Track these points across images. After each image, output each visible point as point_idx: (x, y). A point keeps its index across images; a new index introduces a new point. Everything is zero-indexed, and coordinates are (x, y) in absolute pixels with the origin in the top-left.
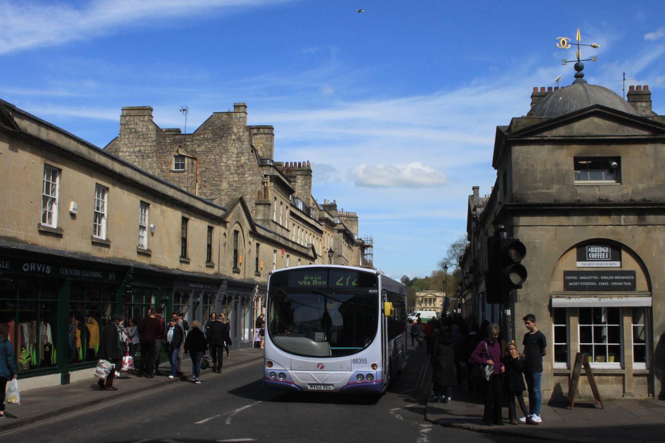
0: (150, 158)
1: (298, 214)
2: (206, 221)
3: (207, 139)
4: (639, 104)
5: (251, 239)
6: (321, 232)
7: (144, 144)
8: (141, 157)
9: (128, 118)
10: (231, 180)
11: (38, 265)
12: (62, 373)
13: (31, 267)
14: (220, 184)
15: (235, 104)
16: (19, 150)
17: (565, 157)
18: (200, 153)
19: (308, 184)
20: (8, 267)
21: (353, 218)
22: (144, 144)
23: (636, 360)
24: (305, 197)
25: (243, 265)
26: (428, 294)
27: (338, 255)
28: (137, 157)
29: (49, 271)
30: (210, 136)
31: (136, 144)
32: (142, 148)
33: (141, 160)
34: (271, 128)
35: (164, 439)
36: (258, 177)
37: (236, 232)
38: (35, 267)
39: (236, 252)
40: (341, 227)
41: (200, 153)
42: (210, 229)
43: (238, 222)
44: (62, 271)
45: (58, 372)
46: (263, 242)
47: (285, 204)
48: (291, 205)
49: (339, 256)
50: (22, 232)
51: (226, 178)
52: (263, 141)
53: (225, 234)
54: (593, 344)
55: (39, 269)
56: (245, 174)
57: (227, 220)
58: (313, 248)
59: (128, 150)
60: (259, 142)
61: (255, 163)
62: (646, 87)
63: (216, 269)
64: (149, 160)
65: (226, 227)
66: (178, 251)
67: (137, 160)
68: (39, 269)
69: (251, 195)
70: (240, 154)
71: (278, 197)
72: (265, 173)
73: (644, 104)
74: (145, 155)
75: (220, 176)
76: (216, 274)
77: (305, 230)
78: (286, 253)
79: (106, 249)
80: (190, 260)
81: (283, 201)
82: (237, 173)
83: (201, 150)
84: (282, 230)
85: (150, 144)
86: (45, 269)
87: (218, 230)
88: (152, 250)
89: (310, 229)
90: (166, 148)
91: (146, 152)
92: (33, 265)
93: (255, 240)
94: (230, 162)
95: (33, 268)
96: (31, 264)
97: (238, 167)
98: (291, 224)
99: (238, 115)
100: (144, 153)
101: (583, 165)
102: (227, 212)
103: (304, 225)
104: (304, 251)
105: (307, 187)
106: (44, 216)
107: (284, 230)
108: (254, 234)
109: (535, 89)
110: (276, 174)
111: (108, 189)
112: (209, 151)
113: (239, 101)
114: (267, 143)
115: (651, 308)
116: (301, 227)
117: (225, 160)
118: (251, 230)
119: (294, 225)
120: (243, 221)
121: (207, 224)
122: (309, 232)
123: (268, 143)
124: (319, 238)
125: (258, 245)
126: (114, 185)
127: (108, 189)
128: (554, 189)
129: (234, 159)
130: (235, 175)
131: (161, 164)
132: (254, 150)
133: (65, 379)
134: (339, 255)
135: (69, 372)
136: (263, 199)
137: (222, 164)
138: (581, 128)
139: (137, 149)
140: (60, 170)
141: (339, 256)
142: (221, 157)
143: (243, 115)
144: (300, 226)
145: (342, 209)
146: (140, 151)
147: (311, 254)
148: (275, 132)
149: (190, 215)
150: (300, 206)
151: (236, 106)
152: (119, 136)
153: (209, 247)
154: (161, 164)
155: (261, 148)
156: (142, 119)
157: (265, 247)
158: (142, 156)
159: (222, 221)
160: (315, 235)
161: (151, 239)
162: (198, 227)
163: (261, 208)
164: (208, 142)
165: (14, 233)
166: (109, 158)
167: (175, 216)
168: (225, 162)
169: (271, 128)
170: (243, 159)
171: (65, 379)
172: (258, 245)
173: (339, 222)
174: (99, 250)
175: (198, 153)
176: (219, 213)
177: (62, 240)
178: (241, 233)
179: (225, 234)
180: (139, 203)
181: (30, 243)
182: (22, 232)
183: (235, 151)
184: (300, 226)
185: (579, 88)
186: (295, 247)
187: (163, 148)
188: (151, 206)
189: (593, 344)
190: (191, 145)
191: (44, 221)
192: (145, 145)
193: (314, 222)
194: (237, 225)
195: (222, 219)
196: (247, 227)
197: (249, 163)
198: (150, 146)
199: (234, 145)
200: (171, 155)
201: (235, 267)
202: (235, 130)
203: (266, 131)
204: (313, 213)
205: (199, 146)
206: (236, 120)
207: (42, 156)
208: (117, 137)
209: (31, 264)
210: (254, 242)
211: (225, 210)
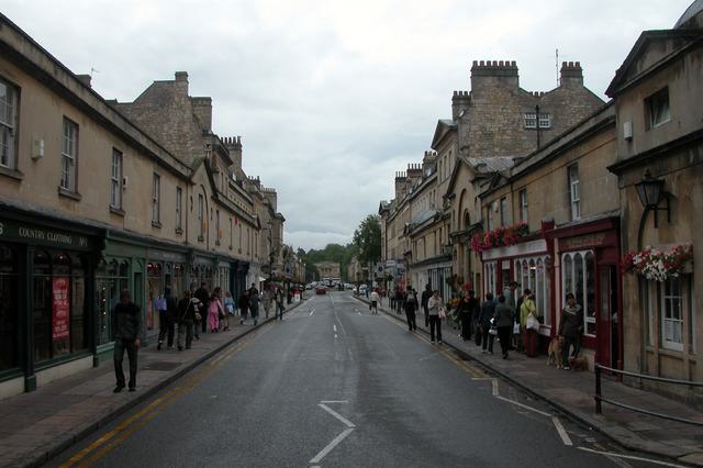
3: (149, 109)
4: (572, 79)
26: (326, 264)
34: (209, 100)
40: (266, 201)
45: (20, 376)
60: (200, 113)
73: (577, 80)
94: (171, 132)
97: (180, 137)
99: (180, 84)
109: (475, 62)
117: (166, 129)
125: (157, 225)
133: (30, 386)
142: (162, 128)
143: (185, 83)
148: (212, 104)
169: (209, 100)
170: (186, 128)
171: (30, 386)
174: (68, 206)
180: (111, 149)
196: (209, 193)
202: (176, 99)
203: (205, 103)
205: (140, 115)
210: (215, 208)
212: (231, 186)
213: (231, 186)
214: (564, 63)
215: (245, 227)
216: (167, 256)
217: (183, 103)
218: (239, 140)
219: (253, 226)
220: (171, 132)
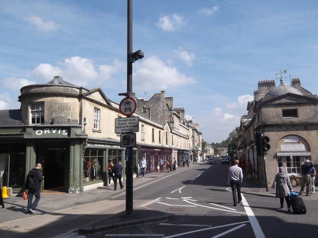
1: (182, 124)
17: (279, 110)
19: (183, 115)
21: (197, 125)
23: (288, 173)
35: (58, 209)
39: (167, 138)
54: (90, 156)
62: (298, 79)
70: (163, 106)
101: (286, 113)
106: (94, 126)
108: (171, 132)
109: (259, 81)
112: (153, 106)
115: (310, 156)
125: (143, 140)
128: (276, 120)
132: (167, 105)
138: (284, 101)
153: (160, 137)
157: (174, 136)
159: (163, 129)
162: (157, 131)
167: (151, 127)
185: (282, 87)
186: (183, 136)
189: (90, 156)
191: (94, 127)
201: (167, 143)
204: (186, 124)
210: (171, 134)
214: (293, 79)
215: (182, 139)
216: (114, 147)
219: (186, 138)
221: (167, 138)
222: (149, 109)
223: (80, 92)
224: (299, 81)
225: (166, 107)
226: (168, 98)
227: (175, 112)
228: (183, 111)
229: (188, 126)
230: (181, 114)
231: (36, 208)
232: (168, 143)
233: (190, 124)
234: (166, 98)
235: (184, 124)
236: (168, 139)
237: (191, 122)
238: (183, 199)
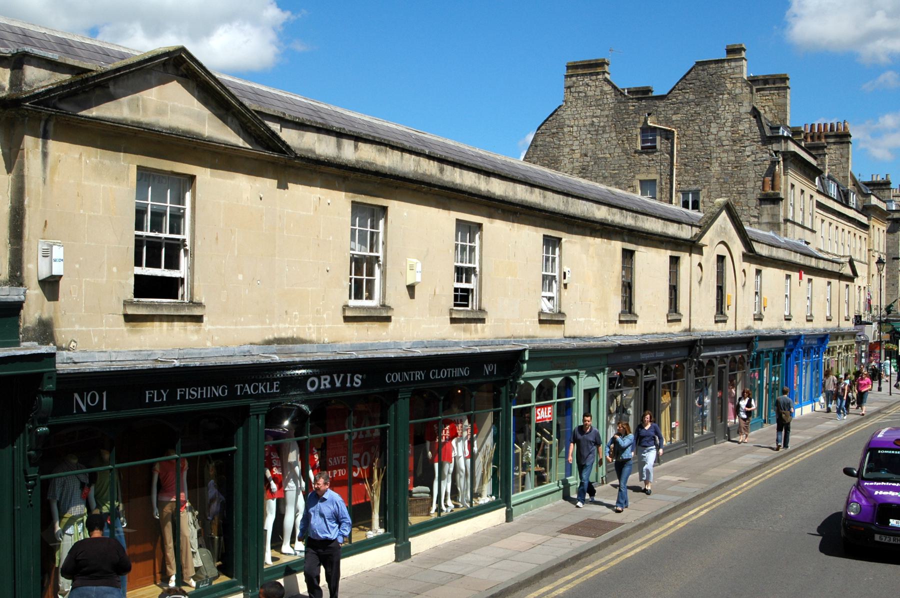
0: (607, 133)
2: (666, 249)
5: (746, 265)
6: (865, 227)
7: (598, 112)
8: (595, 133)
9: (574, 79)
10: (725, 160)
11: (335, 376)
12: (396, 542)
13: (323, 382)
14: (708, 168)
15: (727, 46)
16: (290, 185)
18: (678, 122)
20: (278, 391)
22: (598, 112)
24: (841, 174)
25: (732, 308)
27: (893, 256)
28: (589, 132)
29: (360, 382)
30: (692, 97)
31: (588, 114)
32: (594, 119)
33: (594, 137)
36: (764, 155)
37: (721, 259)
38: (330, 383)
39: (720, 289)
41: (678, 122)
42: (675, 261)
43: (723, 243)
44: (390, 378)
46: (767, 266)
47: (808, 192)
48: (818, 191)
49: (894, 259)
50: (311, 325)
51: (717, 158)
52: (774, 97)
53: (700, 265)
55: (338, 384)
56: (744, 151)
57: (703, 241)
58: (851, 262)
59: (576, 123)
61: (757, 136)
63: (684, 324)
64: (606, 136)
65: (701, 253)
66: (616, 304)
67: (589, 136)
68: (338, 384)
69: (755, 182)
70: (738, 120)
71: (796, 183)
72: (775, 149)
74: (599, 129)
75: (709, 158)
76: (688, 330)
77: (841, 226)
78: (806, 277)
79: (479, 325)
80: (637, 316)
81: (804, 188)
82: (732, 150)
83: (679, 119)
84: (804, 232)
85: (606, 113)
86: (352, 381)
87: (687, 260)
88: (566, 314)
89: (849, 224)
90: (629, 118)
91: (602, 124)
92: (325, 380)
93: (752, 265)
95: (325, 385)
96: (323, 377)
98: (818, 222)
100: (598, 126)
102: (704, 227)
103: (839, 220)
104: (835, 268)
105: (844, 160)
107: (807, 232)
108: (751, 256)
110: (793, 150)
111: (480, 226)
113: (733, 42)
114: (777, 100)
116: (834, 224)
118: (744, 250)
119: (823, 221)
120: (731, 239)
121: (669, 253)
122: (847, 229)
123: (780, 101)
124: (864, 236)
125: (758, 272)
126: (490, 216)
127: (480, 226)
129: (728, 129)
130: (730, 154)
131: (623, 141)
132: (755, 113)
133: (403, 553)
134: (895, 256)
135: (410, 540)
136: (769, 190)
137: (711, 137)
139: (587, 122)
140: (384, 209)
141: (894, 259)
144: (832, 221)
145: (848, 472)
146: (592, 124)
147: (847, 271)
149: (637, 244)
150: (833, 191)
151: (730, 51)
152: (564, 104)
154: (623, 141)
155: (771, 110)
156: (594, 78)
158: (595, 131)
159: (693, 246)
160: (857, 232)
161: (566, 294)
163: (768, 207)
164: (690, 106)
165: (295, 330)
166: (185, 321)
168: (715, 135)
170: (743, 127)
172: (758, 272)
173: (894, 209)
174: (465, 330)
175: (675, 122)
176: (686, 233)
177: (391, 325)
178: (728, 259)
179: (700, 265)
181: (404, 339)
182: (311, 325)
183: (730, 118)
184: (832, 221)
187: (625, 118)
188: (563, 240)
190: (663, 111)
192: (599, 114)
193: (856, 213)
194: (722, 246)
195: (694, 242)
196: (738, 248)
197: (750, 135)
198: (607, 116)
199: (727, 108)
200: (636, 128)
202: (729, 86)
204: (853, 199)
206: (729, 71)
207: (346, 190)
208: (560, 106)
209: (323, 377)
210: (752, 268)
211: (700, 227)
212: (820, 205)
213: (820, 205)
215: (820, 282)
217: (738, 91)
218: (845, 127)
219: (840, 277)
220: (722, 134)
221: (720, 289)
222: (668, 135)
223: (16, 82)
224: (848, 135)
225: (747, 125)
226: (766, 80)
227: (793, 147)
228: (843, 138)
229: (867, 210)
230: (832, 152)
231: (283, 129)
232: (730, 312)
233: (874, 201)
234: (753, 81)
235: (843, 198)
236: (729, 291)
237: (881, 186)
238: (366, 483)
